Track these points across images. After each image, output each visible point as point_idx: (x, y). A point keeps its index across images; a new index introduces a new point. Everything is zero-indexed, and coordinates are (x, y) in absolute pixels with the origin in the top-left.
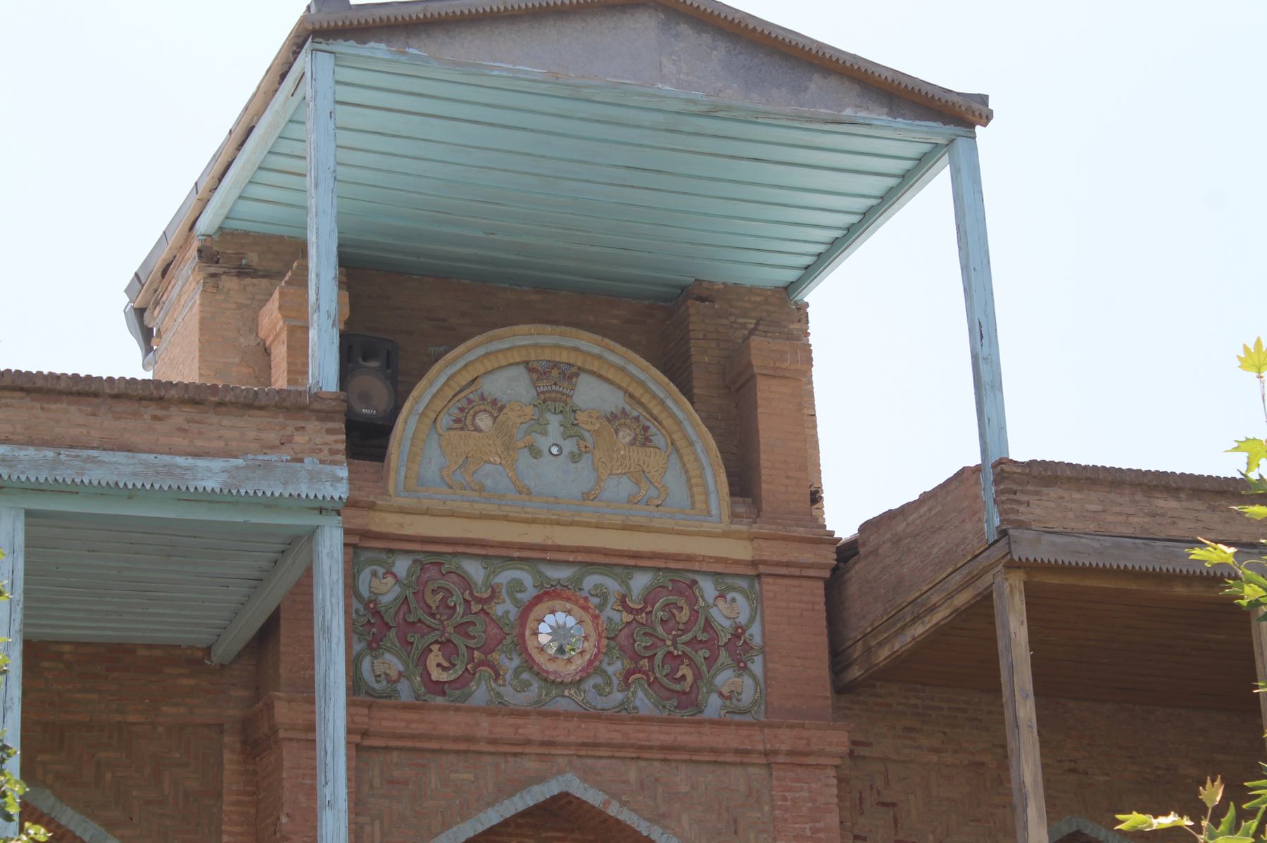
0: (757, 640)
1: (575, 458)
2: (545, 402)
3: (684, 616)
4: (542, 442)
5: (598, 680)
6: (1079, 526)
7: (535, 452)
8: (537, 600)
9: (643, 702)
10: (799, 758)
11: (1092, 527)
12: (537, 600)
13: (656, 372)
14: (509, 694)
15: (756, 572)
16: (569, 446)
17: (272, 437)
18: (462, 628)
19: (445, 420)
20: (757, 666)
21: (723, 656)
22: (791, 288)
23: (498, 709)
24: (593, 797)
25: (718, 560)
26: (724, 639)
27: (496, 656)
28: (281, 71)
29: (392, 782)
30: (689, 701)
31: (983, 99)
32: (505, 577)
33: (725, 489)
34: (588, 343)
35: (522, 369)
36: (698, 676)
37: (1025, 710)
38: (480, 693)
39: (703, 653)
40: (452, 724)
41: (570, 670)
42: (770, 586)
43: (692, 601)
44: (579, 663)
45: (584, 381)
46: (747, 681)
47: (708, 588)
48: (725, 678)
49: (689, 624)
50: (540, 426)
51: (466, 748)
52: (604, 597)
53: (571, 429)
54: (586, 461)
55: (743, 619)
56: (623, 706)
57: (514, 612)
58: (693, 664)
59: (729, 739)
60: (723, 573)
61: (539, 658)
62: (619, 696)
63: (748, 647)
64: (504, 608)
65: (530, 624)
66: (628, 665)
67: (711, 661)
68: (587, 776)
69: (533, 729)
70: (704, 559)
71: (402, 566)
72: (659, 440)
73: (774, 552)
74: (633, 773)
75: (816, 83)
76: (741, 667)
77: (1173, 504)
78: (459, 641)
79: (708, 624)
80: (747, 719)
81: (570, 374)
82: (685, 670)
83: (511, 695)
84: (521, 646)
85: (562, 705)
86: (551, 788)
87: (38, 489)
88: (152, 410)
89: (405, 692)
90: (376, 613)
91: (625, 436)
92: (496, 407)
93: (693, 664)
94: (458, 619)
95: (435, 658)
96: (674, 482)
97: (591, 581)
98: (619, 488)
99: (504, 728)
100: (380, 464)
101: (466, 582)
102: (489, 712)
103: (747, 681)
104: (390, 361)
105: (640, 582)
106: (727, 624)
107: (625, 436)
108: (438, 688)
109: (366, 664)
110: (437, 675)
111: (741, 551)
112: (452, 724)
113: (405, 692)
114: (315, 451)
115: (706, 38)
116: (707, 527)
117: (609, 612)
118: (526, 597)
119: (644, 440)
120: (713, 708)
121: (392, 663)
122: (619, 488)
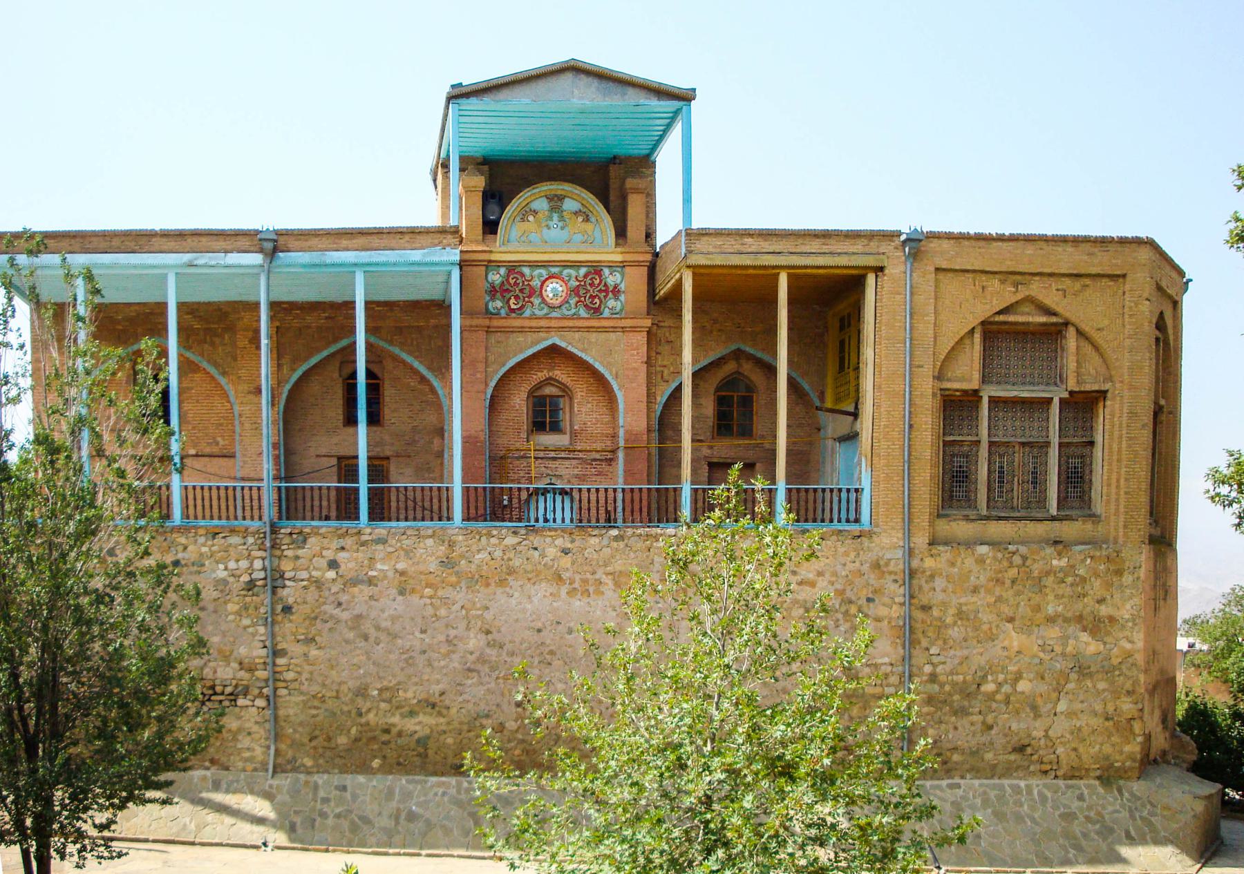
0: (623, 289)
1: (562, 228)
2: (553, 209)
3: (597, 282)
4: (551, 224)
5: (567, 305)
6: (714, 250)
7: (548, 227)
8: (547, 279)
9: (583, 312)
10: (634, 329)
11: (718, 250)
12: (547, 279)
13: (591, 196)
14: (537, 312)
15: (623, 265)
16: (560, 224)
17: (436, 241)
18: (522, 291)
19: (518, 219)
20: (622, 297)
21: (611, 295)
22: (648, 156)
23: (533, 317)
24: (563, 345)
25: (609, 262)
26: (611, 289)
27: (532, 299)
28: (447, 107)
29: (499, 342)
30: (597, 310)
31: (694, 90)
32: (537, 272)
33: (614, 236)
34: (567, 187)
35: (544, 199)
36: (601, 302)
37: (687, 316)
38: (527, 313)
39: (604, 294)
40: (518, 323)
41: (556, 302)
42: (627, 270)
43: (600, 276)
44: (560, 300)
45: (566, 200)
46: (619, 303)
47: (606, 271)
48: (611, 303)
49: (599, 285)
50: (551, 218)
51: (521, 330)
52: (570, 276)
53: (562, 218)
54: (567, 229)
55: (618, 282)
56: (575, 314)
57: (539, 284)
58: (599, 298)
59: (610, 323)
60: (612, 266)
61: (548, 299)
62: (573, 311)
63: (619, 291)
64: (536, 283)
65: (545, 287)
66: (577, 299)
67: (606, 297)
68: (562, 338)
69: (543, 323)
70: (604, 262)
71: (503, 271)
72: (593, 219)
73: (629, 257)
74: (577, 335)
75: (631, 91)
76: (617, 299)
77: (750, 240)
78: (520, 295)
79: (606, 285)
80: (617, 316)
81: (561, 198)
82: (597, 300)
83: (538, 312)
84: (541, 295)
85: (554, 315)
86: (549, 342)
87: (368, 264)
88: (399, 236)
89: (503, 312)
90: (493, 287)
91: (580, 219)
92: (535, 212)
93: (599, 298)
94: (520, 287)
95: (513, 301)
96: (597, 234)
97: (566, 272)
98: (578, 238)
99: (534, 323)
100: (368, 299)
101: (523, 275)
102: (530, 318)
103: (619, 303)
104: (500, 199)
105: (583, 271)
106: (612, 283)
107: (580, 219)
108: (513, 311)
109: (490, 304)
110: (513, 307)
111: (619, 258)
112: (518, 323)
113: (503, 312)
114: (449, 245)
115: (590, 79)
116: (606, 250)
117: (571, 282)
118: (543, 279)
119: (587, 219)
120: (606, 313)
121: (499, 304)
122: (578, 238)
